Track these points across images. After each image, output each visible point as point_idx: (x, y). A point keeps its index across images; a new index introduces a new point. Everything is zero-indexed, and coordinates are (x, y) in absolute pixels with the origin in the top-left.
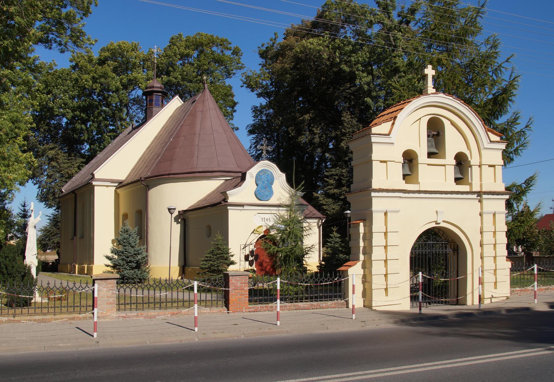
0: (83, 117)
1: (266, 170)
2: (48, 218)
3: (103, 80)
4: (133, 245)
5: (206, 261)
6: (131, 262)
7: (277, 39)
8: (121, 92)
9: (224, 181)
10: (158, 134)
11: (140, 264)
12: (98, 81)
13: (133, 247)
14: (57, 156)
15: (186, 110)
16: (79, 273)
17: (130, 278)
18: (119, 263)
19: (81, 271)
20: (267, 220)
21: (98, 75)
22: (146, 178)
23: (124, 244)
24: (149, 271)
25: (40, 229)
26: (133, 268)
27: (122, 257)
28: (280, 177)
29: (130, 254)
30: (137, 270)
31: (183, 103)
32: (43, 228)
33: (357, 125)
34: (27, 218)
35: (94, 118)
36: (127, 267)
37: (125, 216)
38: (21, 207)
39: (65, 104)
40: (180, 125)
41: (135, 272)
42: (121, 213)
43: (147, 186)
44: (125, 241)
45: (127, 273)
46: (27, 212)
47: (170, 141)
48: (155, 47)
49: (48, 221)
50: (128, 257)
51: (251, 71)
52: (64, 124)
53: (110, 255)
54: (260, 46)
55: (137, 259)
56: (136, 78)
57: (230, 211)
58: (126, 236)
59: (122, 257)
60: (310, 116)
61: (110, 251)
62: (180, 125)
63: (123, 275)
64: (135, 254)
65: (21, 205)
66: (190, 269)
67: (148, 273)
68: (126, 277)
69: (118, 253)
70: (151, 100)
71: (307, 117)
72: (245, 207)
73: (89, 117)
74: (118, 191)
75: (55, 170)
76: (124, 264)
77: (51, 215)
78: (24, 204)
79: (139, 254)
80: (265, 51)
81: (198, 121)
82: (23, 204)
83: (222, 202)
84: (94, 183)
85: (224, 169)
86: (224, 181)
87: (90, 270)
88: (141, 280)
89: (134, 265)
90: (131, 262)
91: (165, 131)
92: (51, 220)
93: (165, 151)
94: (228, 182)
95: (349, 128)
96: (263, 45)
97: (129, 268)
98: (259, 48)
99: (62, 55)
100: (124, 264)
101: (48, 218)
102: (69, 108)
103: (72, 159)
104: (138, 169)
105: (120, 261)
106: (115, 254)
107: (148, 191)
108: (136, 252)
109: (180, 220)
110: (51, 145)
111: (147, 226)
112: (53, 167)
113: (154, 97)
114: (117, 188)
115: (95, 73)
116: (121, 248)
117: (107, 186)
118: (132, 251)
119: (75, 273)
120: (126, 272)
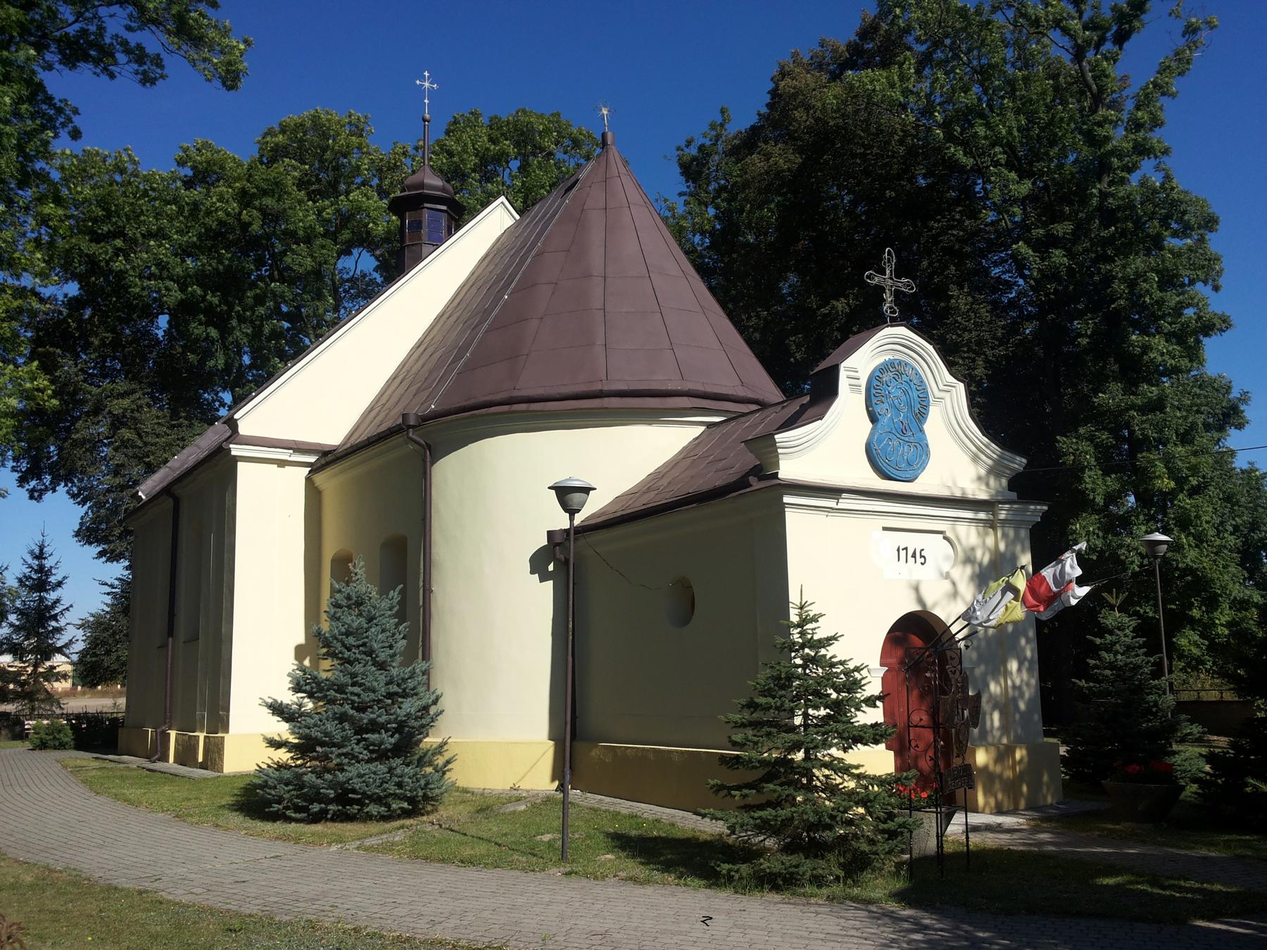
0: (211, 303)
1: (900, 363)
2: (108, 590)
3: (268, 201)
4: (382, 656)
5: (755, 725)
6: (375, 727)
7: (726, 126)
8: (319, 241)
9: (702, 429)
10: (447, 306)
11: (411, 735)
12: (257, 203)
13: (382, 666)
14: (137, 415)
15: (543, 217)
17: (369, 797)
18: (326, 734)
19: (186, 755)
20: (914, 556)
22: (425, 419)
23: (347, 654)
24: (448, 762)
25: (80, 622)
26: (381, 755)
27: (337, 709)
28: (947, 395)
29: (372, 696)
30: (399, 761)
31: (518, 217)
32: (91, 619)
33: (990, 323)
35: (244, 310)
36: (357, 749)
37: (342, 566)
39: (161, 265)
40: (533, 253)
41: (391, 770)
42: (330, 550)
43: (429, 447)
44: (351, 640)
45: (360, 776)
46: (48, 573)
47: (501, 303)
48: (426, 74)
49: (108, 600)
50: (362, 708)
51: (666, 201)
53: (288, 697)
54: (683, 144)
55: (401, 713)
56: (359, 210)
58: (353, 620)
59: (337, 709)
60: (848, 304)
61: (287, 683)
62: (533, 253)
63: (341, 784)
64: (390, 695)
65: (32, 553)
66: (594, 753)
67: (442, 771)
68: (354, 791)
69: (321, 690)
70: (417, 225)
72: (846, 502)
73: (231, 308)
74: (319, 479)
75: (130, 452)
76: (346, 739)
77: (117, 583)
78: (42, 548)
79: (405, 695)
80: (694, 159)
81: (596, 236)
82: (37, 551)
83: (752, 479)
84: (236, 450)
85: (698, 387)
86: (702, 429)
87: (215, 752)
88: (418, 804)
89: (390, 741)
90: (375, 727)
91: (474, 290)
92: (115, 598)
93: (486, 332)
94: (718, 432)
96: (689, 143)
97: (365, 755)
98: (678, 149)
99: (150, 91)
100: (346, 739)
101: (108, 590)
103: (180, 426)
105: (330, 726)
106: (311, 695)
107: (433, 463)
108: (394, 688)
109: (551, 568)
110: (122, 385)
111: (428, 591)
112: (125, 443)
113: (426, 215)
114: (315, 469)
115: (248, 181)
116: (327, 670)
117: (282, 463)
118: (378, 680)
119: (167, 761)
120: (353, 771)
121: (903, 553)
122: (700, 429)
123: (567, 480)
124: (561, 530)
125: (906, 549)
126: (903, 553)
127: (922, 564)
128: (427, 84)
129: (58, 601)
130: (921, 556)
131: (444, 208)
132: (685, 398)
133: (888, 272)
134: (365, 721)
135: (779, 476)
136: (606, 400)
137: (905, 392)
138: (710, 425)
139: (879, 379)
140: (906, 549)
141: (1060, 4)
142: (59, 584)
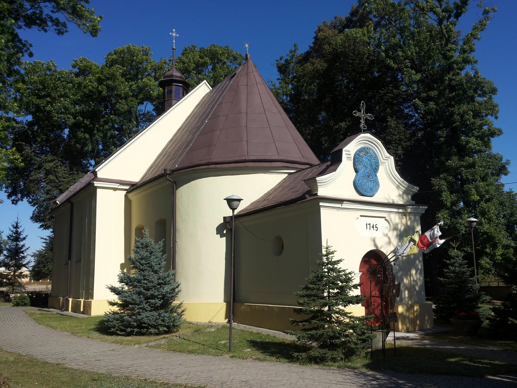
0: (86, 124)
1: (367, 148)
2: (44, 241)
3: (110, 82)
4: (156, 268)
5: (308, 296)
6: (153, 297)
7: (296, 51)
9: (286, 175)
11: (168, 300)
12: (105, 83)
13: (156, 272)
14: (56, 169)
16: (73, 310)
17: (151, 326)
18: (133, 300)
19: (76, 308)
20: (373, 227)
21: (105, 77)
22: (173, 171)
23: (142, 267)
24: (183, 311)
26: (156, 308)
27: (137, 289)
28: (386, 161)
29: (152, 284)
30: (163, 311)
31: (211, 89)
32: (37, 253)
34: (19, 241)
36: (146, 306)
37: (140, 231)
38: (12, 229)
40: (218, 103)
41: (159, 315)
42: (134, 225)
43: (175, 183)
44: (143, 262)
45: (147, 317)
46: (20, 234)
47: (205, 124)
48: (174, 30)
49: (44, 245)
50: (148, 289)
51: (272, 82)
52: (65, 136)
53: (118, 285)
54: (279, 59)
55: (164, 291)
57: (323, 211)
58: (144, 253)
59: (137, 289)
60: (346, 124)
61: (117, 279)
63: (139, 320)
64: (159, 284)
65: (13, 226)
66: (243, 308)
67: (180, 315)
68: (144, 323)
69: (131, 282)
70: (170, 92)
71: (343, 125)
72: (345, 205)
74: (130, 196)
75: (53, 184)
76: (141, 302)
77: (48, 238)
78: (17, 224)
79: (165, 284)
82: (15, 225)
83: (307, 196)
84: (96, 184)
86: (286, 175)
87: (88, 307)
88: (170, 329)
89: (159, 303)
90: (153, 297)
91: (193, 119)
92: (47, 244)
93: (198, 135)
94: (293, 177)
95: (396, 135)
96: (281, 58)
97: (149, 308)
98: (277, 61)
99: (61, 37)
100: (141, 302)
101: (44, 241)
102: (70, 114)
103: (73, 174)
104: (158, 165)
105: (135, 297)
107: (177, 189)
108: (161, 281)
109: (225, 232)
110: (50, 157)
111: (175, 241)
112: (51, 181)
113: (174, 88)
114: (128, 192)
115: (101, 74)
116: (133, 274)
117: (115, 189)
118: (154, 278)
119: (68, 311)
121: (368, 226)
122: (286, 175)
123: (231, 196)
124: (229, 216)
125: (370, 224)
126: (368, 226)
127: (376, 230)
128: (174, 34)
129: (23, 245)
130: (376, 227)
131: (181, 85)
132: (280, 163)
133: (362, 111)
134: (149, 295)
135: (318, 195)
136: (247, 163)
137: (369, 160)
138: (290, 174)
139: (359, 155)
140: (370, 224)
141: (432, 2)
142: (24, 238)
